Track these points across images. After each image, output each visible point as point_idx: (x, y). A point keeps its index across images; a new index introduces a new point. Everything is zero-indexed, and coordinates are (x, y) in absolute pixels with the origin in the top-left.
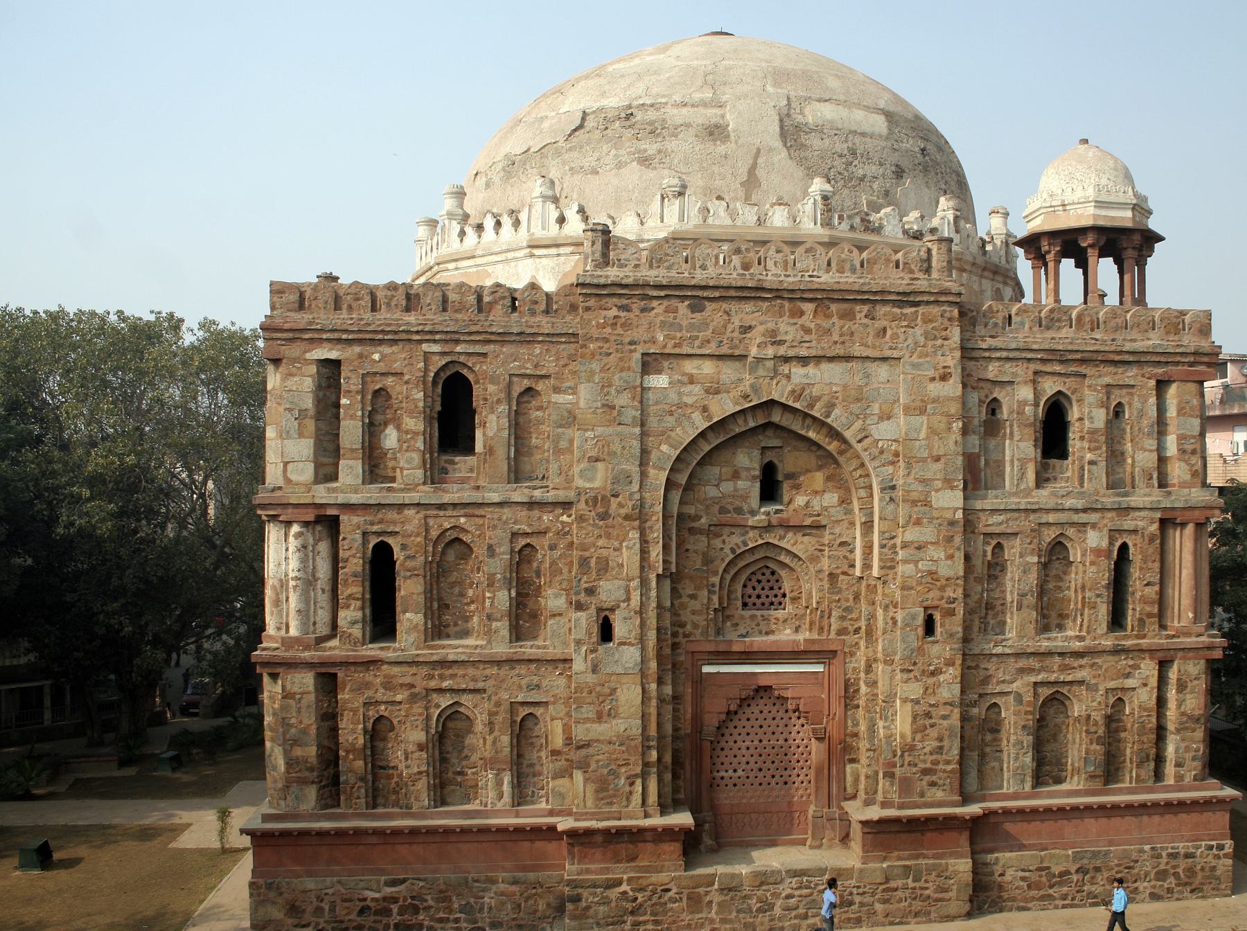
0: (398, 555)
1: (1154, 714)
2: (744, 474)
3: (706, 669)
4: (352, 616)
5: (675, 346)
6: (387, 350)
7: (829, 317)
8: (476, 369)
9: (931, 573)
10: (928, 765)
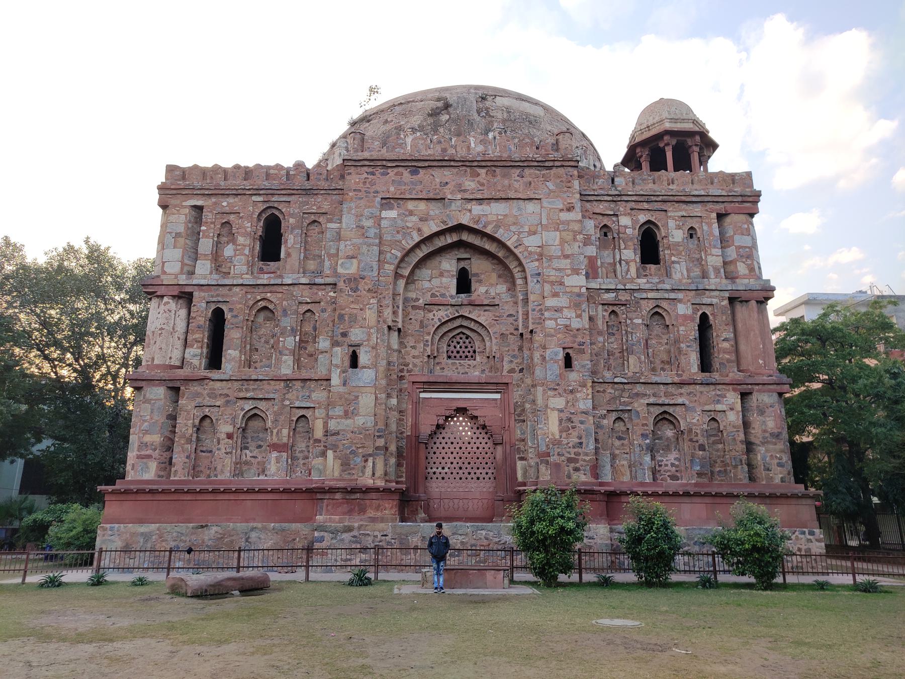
0: (228, 316)
1: (742, 429)
2: (446, 274)
4: (196, 355)
6: (231, 200)
9: (566, 326)
10: (573, 456)
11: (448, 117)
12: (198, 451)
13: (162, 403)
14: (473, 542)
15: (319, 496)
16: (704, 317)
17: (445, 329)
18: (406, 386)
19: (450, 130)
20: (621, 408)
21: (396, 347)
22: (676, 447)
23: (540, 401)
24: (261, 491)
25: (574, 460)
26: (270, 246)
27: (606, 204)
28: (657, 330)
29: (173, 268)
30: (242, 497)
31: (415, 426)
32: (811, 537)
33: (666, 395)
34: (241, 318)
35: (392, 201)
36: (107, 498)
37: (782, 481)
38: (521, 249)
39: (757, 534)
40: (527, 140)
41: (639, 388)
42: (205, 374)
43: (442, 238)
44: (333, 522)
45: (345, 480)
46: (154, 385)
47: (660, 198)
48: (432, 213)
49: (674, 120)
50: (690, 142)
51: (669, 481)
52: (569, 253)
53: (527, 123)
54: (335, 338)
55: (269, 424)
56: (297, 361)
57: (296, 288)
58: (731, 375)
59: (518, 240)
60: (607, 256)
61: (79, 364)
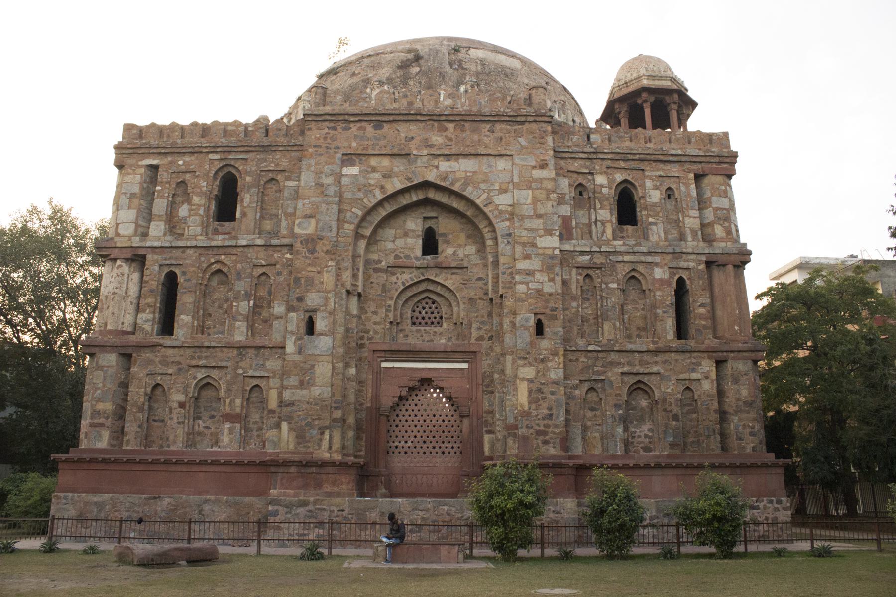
0: (181, 279)
1: (716, 398)
2: (410, 234)
3: (385, 365)
4: (148, 320)
5: (364, 149)
6: (187, 158)
7: (463, 131)
8: (240, 168)
9: (538, 291)
10: (542, 428)
11: (418, 69)
12: (151, 421)
13: (114, 370)
14: (434, 518)
15: (273, 469)
16: (681, 282)
17: (409, 293)
18: (366, 354)
19: (420, 83)
21: (355, 312)
22: (650, 417)
23: (509, 371)
24: (213, 463)
25: (544, 433)
26: (226, 207)
27: (581, 162)
28: (633, 294)
29: (127, 230)
30: (195, 468)
31: (376, 397)
32: (778, 506)
34: (194, 281)
35: (354, 157)
36: (60, 466)
37: (754, 451)
38: (491, 208)
39: (718, 504)
40: (498, 94)
41: (613, 357)
42: (158, 341)
43: (407, 196)
44: (288, 496)
45: (299, 453)
47: (637, 157)
48: (396, 169)
49: (651, 77)
50: (668, 99)
51: (642, 452)
52: (542, 212)
53: (503, 76)
54: (291, 303)
55: (222, 393)
56: (251, 328)
57: (251, 250)
58: (707, 342)
59: (488, 198)
60: (582, 216)
61: (41, 330)
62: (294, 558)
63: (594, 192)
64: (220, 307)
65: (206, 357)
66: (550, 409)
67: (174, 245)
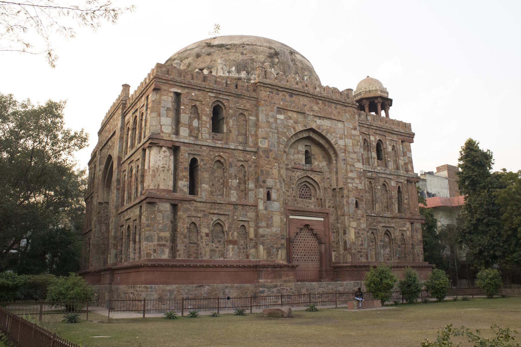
2: (300, 153)
3: (291, 217)
4: (184, 184)
8: (225, 104)
9: (356, 187)
11: (278, 60)
16: (399, 187)
19: (280, 68)
20: (373, 228)
23: (347, 224)
27: (365, 129)
30: (220, 270)
33: (389, 222)
45: (269, 261)
46: (163, 202)
47: (384, 130)
48: (299, 120)
55: (226, 229)
57: (236, 151)
62: (232, 314)
63: (370, 144)
64: (219, 181)
65: (218, 209)
66: (362, 241)
67: (196, 143)
